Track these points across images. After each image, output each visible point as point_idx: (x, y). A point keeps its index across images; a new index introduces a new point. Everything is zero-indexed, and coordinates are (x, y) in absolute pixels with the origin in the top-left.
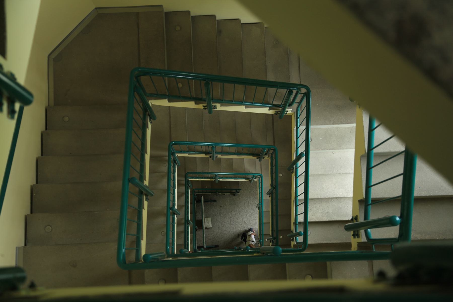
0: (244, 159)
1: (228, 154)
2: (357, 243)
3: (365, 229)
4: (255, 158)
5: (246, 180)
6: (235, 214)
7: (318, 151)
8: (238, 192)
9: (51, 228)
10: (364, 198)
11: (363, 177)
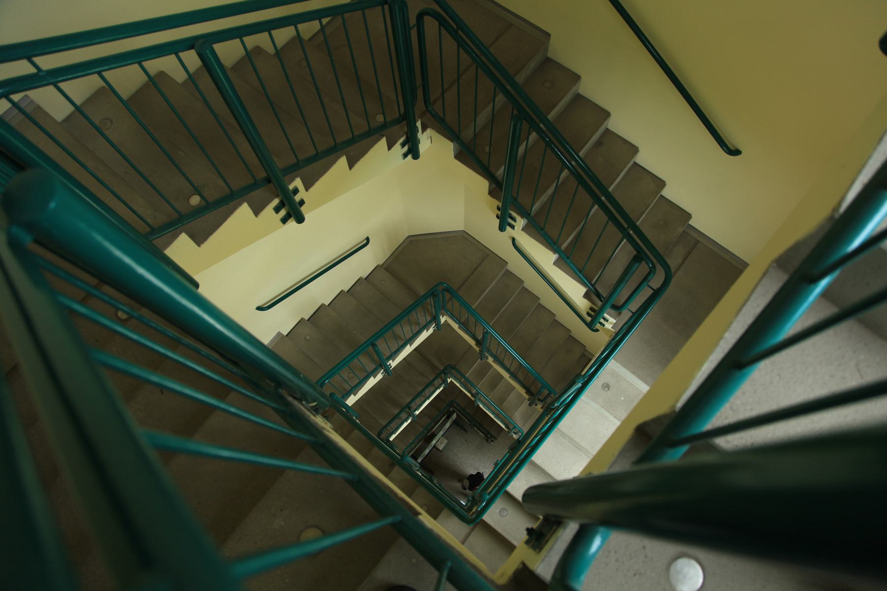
0: (515, 388)
1: (500, 364)
2: (521, 566)
3: (585, 521)
4: (527, 396)
5: (505, 428)
6: (473, 459)
7: (604, 411)
8: (492, 441)
9: (108, 126)
10: (674, 411)
11: (727, 335)
